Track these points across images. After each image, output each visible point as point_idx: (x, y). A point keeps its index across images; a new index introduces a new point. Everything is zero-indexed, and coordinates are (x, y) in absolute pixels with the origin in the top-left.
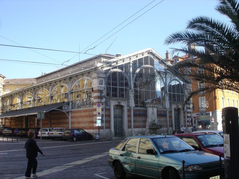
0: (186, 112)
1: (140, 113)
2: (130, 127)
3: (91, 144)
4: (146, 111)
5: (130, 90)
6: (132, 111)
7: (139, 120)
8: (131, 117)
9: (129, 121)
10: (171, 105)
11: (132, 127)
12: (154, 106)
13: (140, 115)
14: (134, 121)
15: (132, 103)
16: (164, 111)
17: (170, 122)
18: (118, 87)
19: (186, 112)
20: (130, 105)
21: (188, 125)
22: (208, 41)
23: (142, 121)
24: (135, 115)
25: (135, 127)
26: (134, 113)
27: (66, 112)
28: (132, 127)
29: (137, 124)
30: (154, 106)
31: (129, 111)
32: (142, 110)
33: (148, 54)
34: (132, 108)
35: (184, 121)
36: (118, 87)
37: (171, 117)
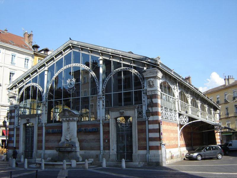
2: (40, 148)
3: (221, 175)
6: (44, 128)
7: (53, 139)
8: (42, 136)
9: (40, 141)
11: (44, 148)
12: (68, 119)
13: (54, 133)
14: (47, 141)
16: (94, 125)
17: (107, 141)
18: (123, 92)
20: (98, 118)
21: (149, 147)
22: (35, 52)
23: (57, 140)
24: (47, 134)
25: (47, 148)
26: (47, 131)
27: (189, 122)
28: (44, 148)
29: (50, 145)
30: (68, 119)
31: (40, 128)
32: (57, 126)
33: (71, 49)
34: (44, 125)
35: (19, 143)
36: (112, 93)
37: (107, 133)
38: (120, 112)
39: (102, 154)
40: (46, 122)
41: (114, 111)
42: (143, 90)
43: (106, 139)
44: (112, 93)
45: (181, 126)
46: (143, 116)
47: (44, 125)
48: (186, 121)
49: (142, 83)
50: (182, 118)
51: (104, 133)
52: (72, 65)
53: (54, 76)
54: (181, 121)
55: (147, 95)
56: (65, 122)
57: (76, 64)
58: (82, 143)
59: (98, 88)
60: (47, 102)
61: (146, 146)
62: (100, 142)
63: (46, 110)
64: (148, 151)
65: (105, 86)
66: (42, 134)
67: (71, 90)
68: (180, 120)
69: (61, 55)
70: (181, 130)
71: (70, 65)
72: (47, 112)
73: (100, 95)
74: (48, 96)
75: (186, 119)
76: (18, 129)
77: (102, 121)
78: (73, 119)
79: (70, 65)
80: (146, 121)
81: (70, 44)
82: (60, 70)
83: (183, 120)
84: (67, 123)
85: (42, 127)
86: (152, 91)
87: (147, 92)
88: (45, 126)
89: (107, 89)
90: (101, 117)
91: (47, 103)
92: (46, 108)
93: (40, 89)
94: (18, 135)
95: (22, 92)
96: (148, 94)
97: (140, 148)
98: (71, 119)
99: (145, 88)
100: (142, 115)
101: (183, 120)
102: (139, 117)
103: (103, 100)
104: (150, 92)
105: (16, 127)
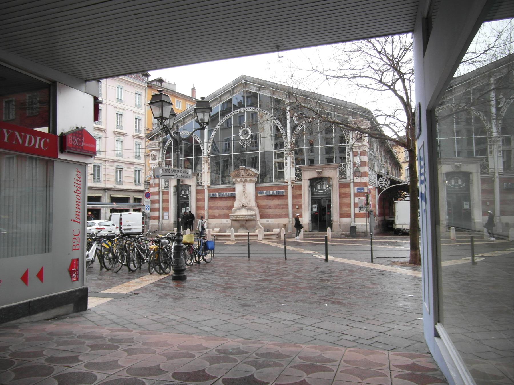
0: (352, 184)
1: (271, 192)
4: (234, 189)
5: (488, 140)
8: (204, 201)
10: (298, 176)
15: (206, 179)
19: (352, 184)
20: (203, 183)
24: (212, 198)
29: (216, 212)
30: (243, 179)
31: (199, 192)
34: (206, 187)
38: (317, 172)
39: (291, 222)
40: (209, 183)
41: (308, 171)
42: (348, 145)
43: (297, 205)
44: (220, 155)
45: (380, 190)
46: (347, 177)
47: (206, 187)
48: (386, 185)
49: (202, 150)
50: (382, 180)
51: (294, 197)
52: (245, 109)
53: (219, 123)
54: (380, 184)
55: (353, 151)
56: (249, 182)
57: (252, 108)
58: (263, 210)
59: (284, 140)
60: (209, 157)
61: (350, 214)
62: (288, 208)
63: (209, 168)
64: (353, 220)
65: (166, 151)
66: (204, 199)
67: (246, 143)
68: (379, 182)
69: (229, 95)
70: (379, 195)
71: (242, 109)
72: (210, 170)
73: (205, 157)
74: (210, 150)
75: (386, 182)
76: (165, 193)
77: (292, 183)
78: (250, 179)
79: (243, 109)
80: (350, 183)
81: (243, 81)
82: (227, 116)
83: (384, 182)
84: (243, 184)
85: (204, 190)
86: (359, 147)
87: (353, 148)
88: (208, 189)
89: (214, 149)
90: (206, 182)
91: (210, 158)
92: (209, 165)
93: (197, 140)
94: (166, 201)
95: (169, 143)
96: (354, 150)
97: (342, 216)
98: (248, 179)
99: (351, 143)
100: (488, 170)
101: (384, 182)
102: (482, 173)
103: (292, 157)
104: (357, 147)
105: (163, 190)
